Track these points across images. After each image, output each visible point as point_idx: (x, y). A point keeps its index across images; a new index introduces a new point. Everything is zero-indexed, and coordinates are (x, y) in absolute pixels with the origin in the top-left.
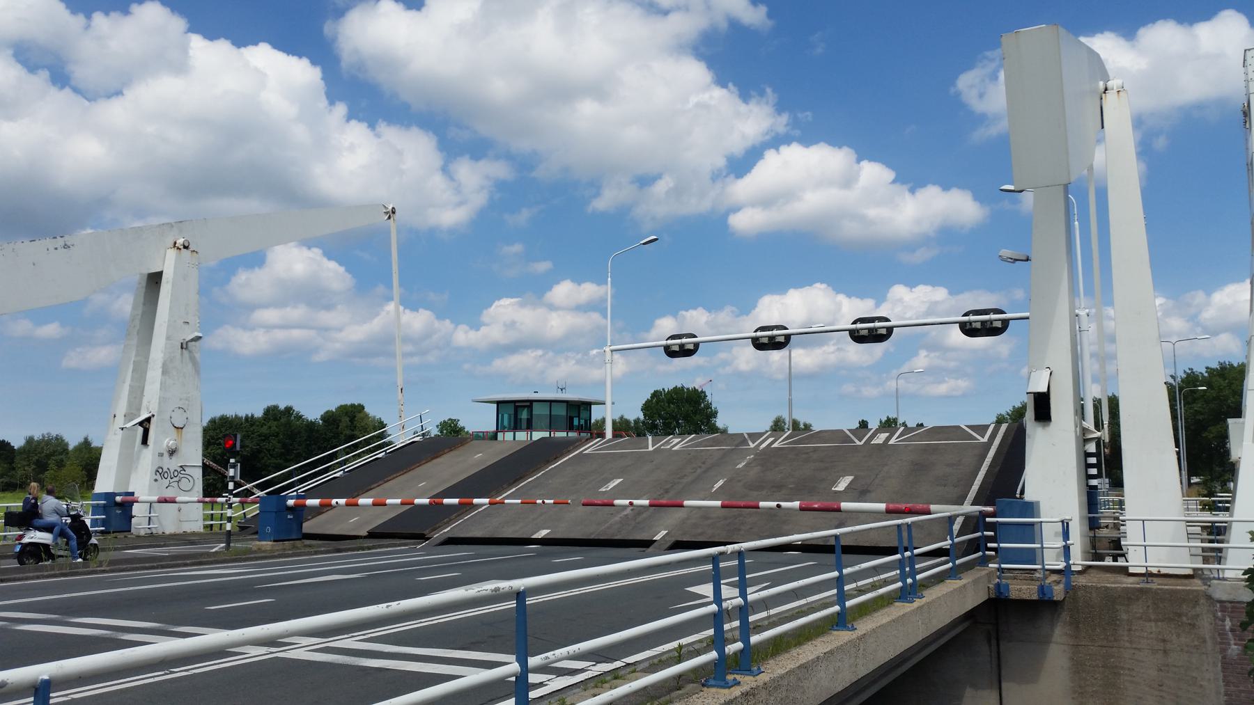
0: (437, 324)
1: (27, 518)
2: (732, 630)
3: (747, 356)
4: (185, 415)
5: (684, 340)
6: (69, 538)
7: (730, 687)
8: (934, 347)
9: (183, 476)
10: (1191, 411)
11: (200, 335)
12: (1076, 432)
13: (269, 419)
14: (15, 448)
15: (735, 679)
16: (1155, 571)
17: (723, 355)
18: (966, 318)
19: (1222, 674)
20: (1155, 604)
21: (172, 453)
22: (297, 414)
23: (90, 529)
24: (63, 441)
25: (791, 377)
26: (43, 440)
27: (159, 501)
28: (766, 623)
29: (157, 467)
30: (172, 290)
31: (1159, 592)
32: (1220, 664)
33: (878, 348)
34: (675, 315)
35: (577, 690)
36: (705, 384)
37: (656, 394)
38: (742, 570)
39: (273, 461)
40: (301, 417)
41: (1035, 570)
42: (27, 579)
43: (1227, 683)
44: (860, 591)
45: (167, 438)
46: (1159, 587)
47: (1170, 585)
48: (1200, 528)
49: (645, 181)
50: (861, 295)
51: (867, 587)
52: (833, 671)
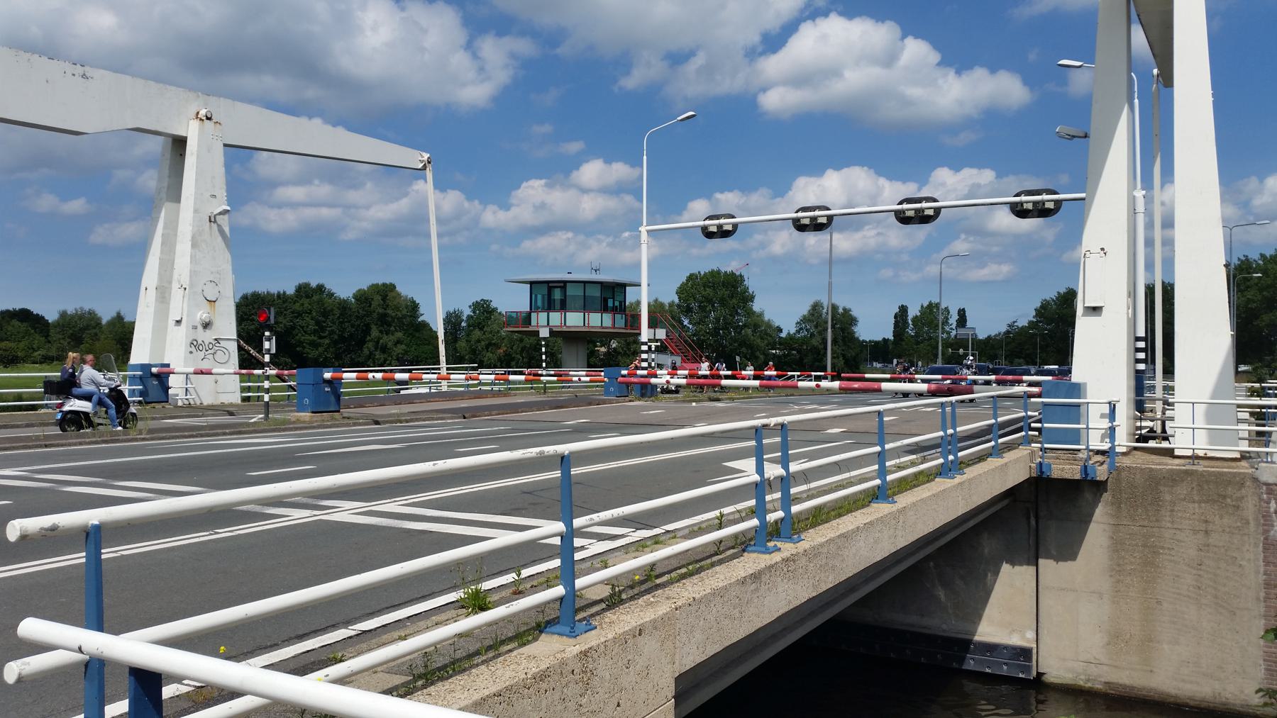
0: (466, 204)
1: (66, 387)
2: (773, 501)
3: (785, 240)
4: (217, 289)
5: (722, 221)
6: (107, 407)
7: (770, 553)
8: (979, 232)
9: (218, 348)
10: (1243, 299)
11: (229, 208)
12: (1128, 313)
13: (302, 296)
14: (50, 321)
15: (775, 546)
16: (1201, 453)
17: (758, 237)
18: (1017, 199)
19: (1262, 555)
20: (1199, 485)
21: (206, 325)
22: (329, 292)
23: (128, 399)
24: (96, 315)
25: (831, 261)
26: (76, 314)
27: (195, 373)
28: (805, 495)
29: (191, 339)
30: (197, 162)
31: (1205, 474)
32: (1261, 545)
33: (921, 231)
34: (708, 196)
35: (621, 553)
36: (741, 269)
37: (691, 277)
38: (784, 447)
39: (308, 337)
40: (333, 294)
41: (1079, 450)
42: (70, 445)
43: (1267, 563)
44: (899, 467)
45: (201, 310)
46: (1205, 469)
47: (1217, 468)
48: (1248, 414)
49: (677, 58)
50: (904, 179)
51: (906, 464)
52: (872, 540)
